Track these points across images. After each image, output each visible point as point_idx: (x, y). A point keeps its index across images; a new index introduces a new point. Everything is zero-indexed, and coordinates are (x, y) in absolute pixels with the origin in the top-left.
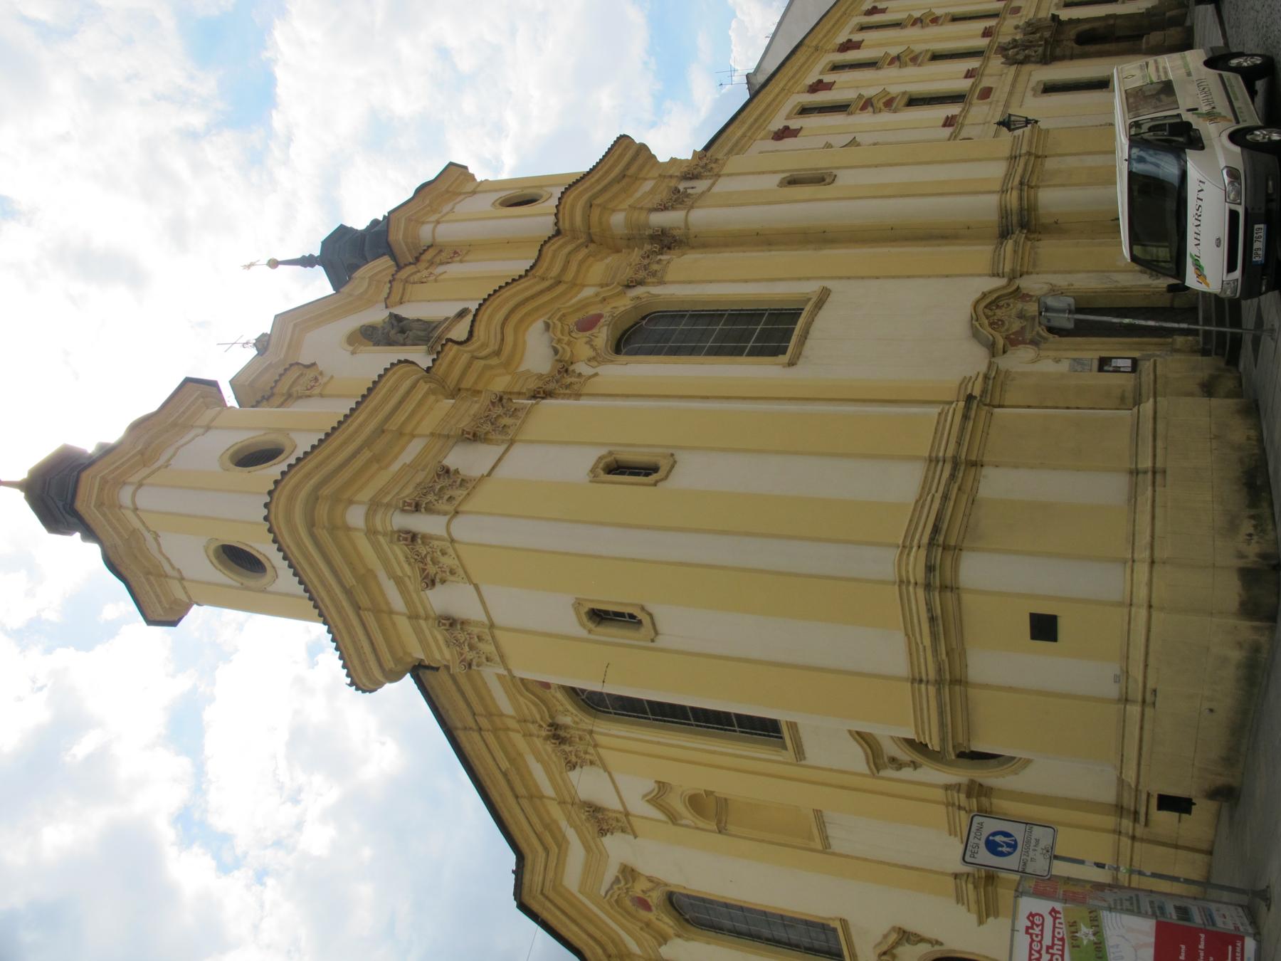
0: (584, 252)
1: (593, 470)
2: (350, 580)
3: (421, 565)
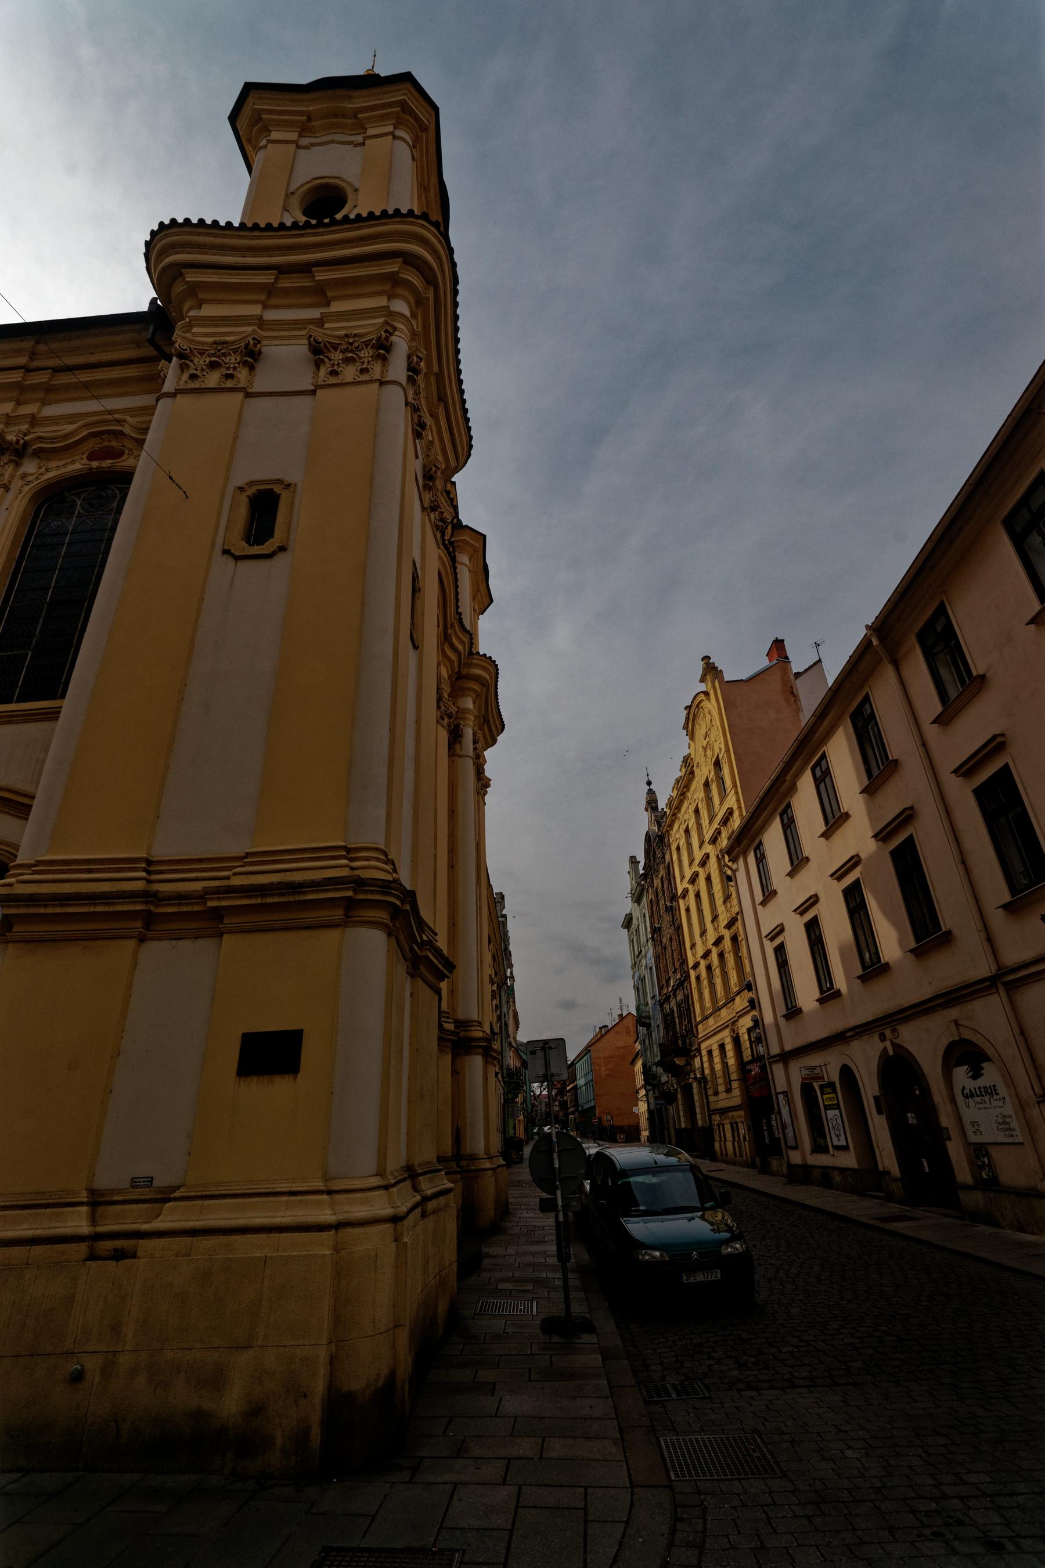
2: (322, 275)
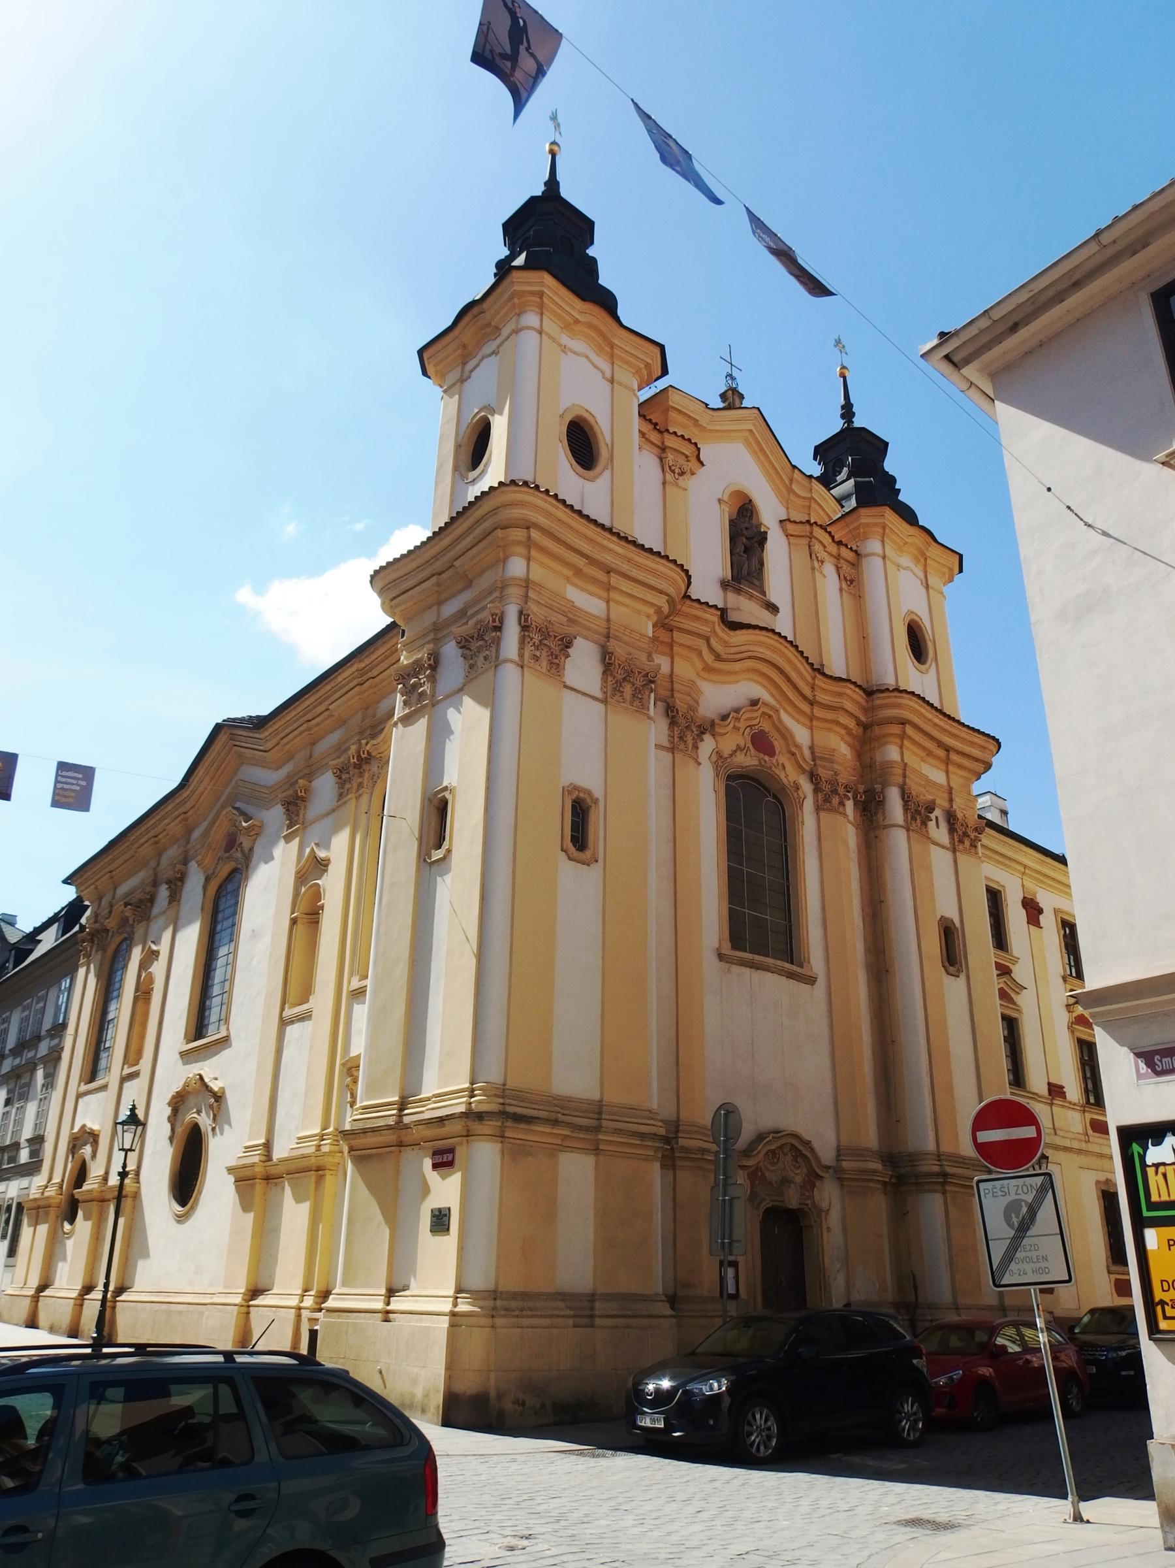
0: (851, 724)
1: (576, 788)
3: (476, 635)
